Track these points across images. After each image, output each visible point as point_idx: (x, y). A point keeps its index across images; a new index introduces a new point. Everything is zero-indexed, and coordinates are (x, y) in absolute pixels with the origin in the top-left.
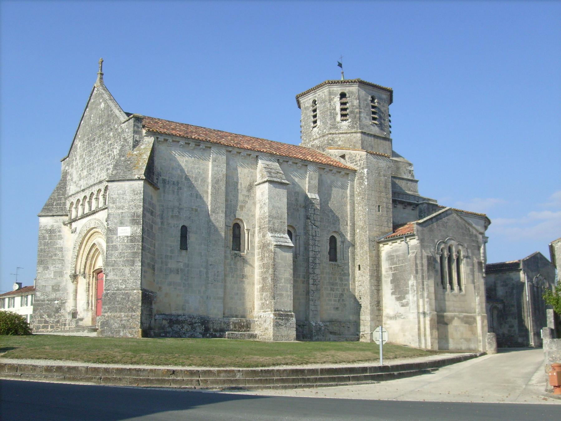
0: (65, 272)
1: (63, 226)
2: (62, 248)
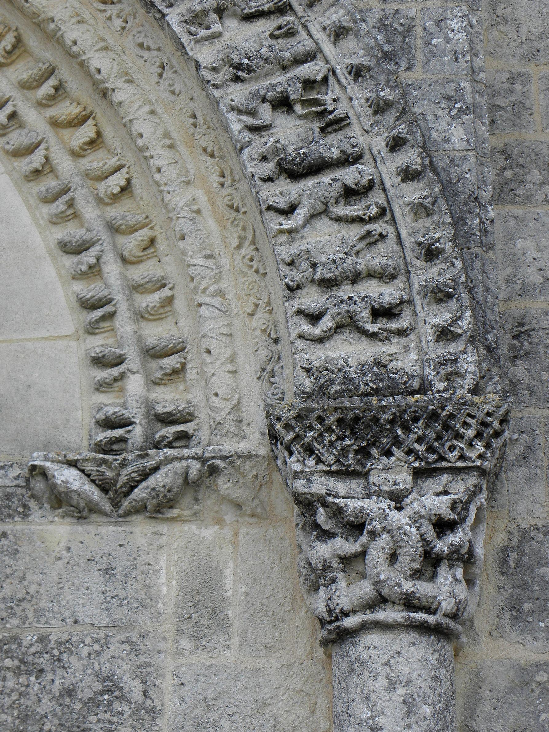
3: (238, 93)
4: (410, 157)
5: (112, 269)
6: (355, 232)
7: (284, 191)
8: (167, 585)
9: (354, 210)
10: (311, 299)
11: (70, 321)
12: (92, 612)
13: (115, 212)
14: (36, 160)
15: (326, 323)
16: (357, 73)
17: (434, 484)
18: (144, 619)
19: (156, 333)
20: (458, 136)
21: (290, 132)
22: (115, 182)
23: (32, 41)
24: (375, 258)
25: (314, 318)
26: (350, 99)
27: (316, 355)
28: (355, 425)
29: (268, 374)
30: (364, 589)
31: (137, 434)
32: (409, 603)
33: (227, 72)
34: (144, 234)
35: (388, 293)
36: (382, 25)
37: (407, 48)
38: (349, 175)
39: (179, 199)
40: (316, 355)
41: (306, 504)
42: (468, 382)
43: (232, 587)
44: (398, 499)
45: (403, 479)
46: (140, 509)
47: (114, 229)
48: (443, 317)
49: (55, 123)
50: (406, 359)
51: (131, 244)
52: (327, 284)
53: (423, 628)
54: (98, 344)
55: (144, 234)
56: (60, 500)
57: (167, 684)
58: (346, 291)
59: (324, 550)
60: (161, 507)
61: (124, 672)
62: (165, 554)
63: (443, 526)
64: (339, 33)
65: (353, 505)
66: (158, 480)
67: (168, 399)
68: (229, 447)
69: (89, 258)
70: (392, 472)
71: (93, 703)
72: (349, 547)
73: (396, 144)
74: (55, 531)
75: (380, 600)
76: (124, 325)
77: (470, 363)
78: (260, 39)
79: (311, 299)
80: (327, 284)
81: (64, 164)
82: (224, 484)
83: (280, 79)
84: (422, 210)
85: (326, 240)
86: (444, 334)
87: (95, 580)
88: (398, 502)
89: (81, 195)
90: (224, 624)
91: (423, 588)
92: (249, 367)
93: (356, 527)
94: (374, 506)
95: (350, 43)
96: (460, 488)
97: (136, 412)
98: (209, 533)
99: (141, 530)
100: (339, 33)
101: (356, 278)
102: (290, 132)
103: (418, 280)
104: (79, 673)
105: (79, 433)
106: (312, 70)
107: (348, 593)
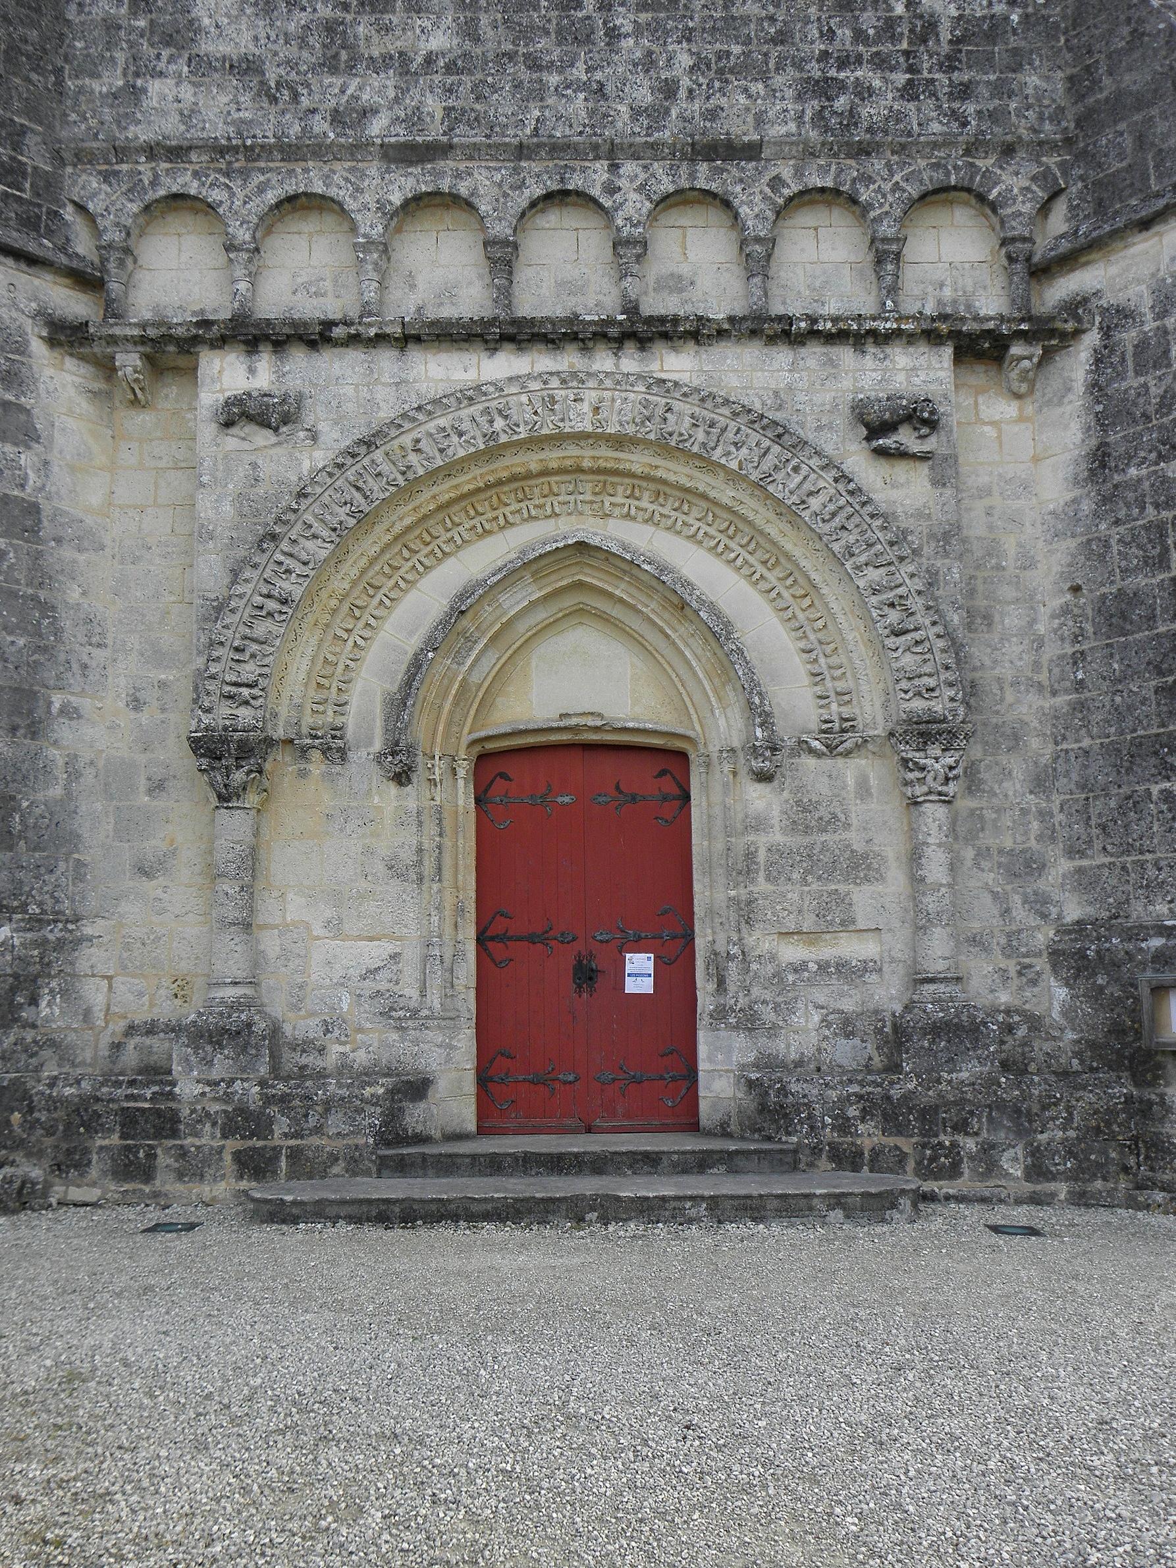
0: (57, 700)
1: (38, 347)
2: (33, 509)
3: (874, 600)
4: (939, 629)
5: (822, 660)
6: (919, 658)
7: (891, 642)
8: (850, 782)
9: (919, 649)
10: (904, 684)
11: (806, 680)
12: (825, 791)
13: (820, 635)
14: (789, 613)
15: (911, 694)
16: (919, 593)
17: (948, 754)
18: (844, 793)
19: (841, 685)
20: (956, 618)
21: (894, 616)
22: (820, 623)
23: (783, 560)
24: (927, 669)
25: (906, 692)
26: (916, 604)
27: (905, 705)
28: (925, 731)
29: (885, 706)
30: (925, 789)
31: (837, 726)
32: (940, 794)
33: (870, 591)
34: (832, 646)
35: (931, 682)
36: (928, 571)
37: (937, 581)
38: (917, 635)
39: (850, 637)
40: (905, 705)
41: (905, 761)
42: (961, 718)
43: (873, 782)
44: (937, 759)
45: (939, 752)
46: (841, 754)
47: (820, 643)
48: (952, 693)
49: (794, 596)
50: (938, 707)
51: (829, 649)
52: (910, 679)
53: (944, 802)
54: (818, 690)
55: (832, 646)
56: (812, 751)
57: (853, 815)
58: (916, 682)
59: (911, 776)
60: (847, 754)
61: (838, 811)
62: (850, 770)
63: (951, 768)
64: (912, 576)
65: (922, 761)
66: (848, 745)
67: (846, 712)
68: (871, 733)
69: (813, 655)
70: (935, 750)
71: (829, 822)
72: (921, 776)
73: (934, 623)
74: (810, 762)
75: (930, 793)
76: (829, 684)
77: (961, 711)
78: (960, 669)
79: (904, 684)
80: (910, 679)
81: (801, 616)
82: (870, 746)
83: (891, 595)
84: (943, 651)
85: (908, 661)
86: (952, 700)
87: (825, 780)
88: (937, 760)
89: (808, 629)
90: (871, 795)
91: (944, 789)
92: (878, 704)
93: (923, 769)
94: (929, 762)
95: (916, 580)
96: (957, 755)
97: (835, 718)
98: (863, 762)
99: (840, 761)
100: (912, 576)
101: (920, 676)
102: (894, 616)
103: (942, 678)
104: (823, 812)
105: (814, 725)
106: (901, 591)
107: (919, 790)
